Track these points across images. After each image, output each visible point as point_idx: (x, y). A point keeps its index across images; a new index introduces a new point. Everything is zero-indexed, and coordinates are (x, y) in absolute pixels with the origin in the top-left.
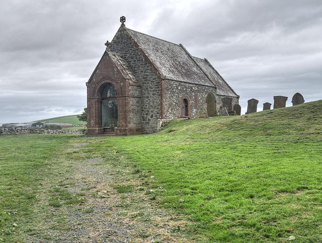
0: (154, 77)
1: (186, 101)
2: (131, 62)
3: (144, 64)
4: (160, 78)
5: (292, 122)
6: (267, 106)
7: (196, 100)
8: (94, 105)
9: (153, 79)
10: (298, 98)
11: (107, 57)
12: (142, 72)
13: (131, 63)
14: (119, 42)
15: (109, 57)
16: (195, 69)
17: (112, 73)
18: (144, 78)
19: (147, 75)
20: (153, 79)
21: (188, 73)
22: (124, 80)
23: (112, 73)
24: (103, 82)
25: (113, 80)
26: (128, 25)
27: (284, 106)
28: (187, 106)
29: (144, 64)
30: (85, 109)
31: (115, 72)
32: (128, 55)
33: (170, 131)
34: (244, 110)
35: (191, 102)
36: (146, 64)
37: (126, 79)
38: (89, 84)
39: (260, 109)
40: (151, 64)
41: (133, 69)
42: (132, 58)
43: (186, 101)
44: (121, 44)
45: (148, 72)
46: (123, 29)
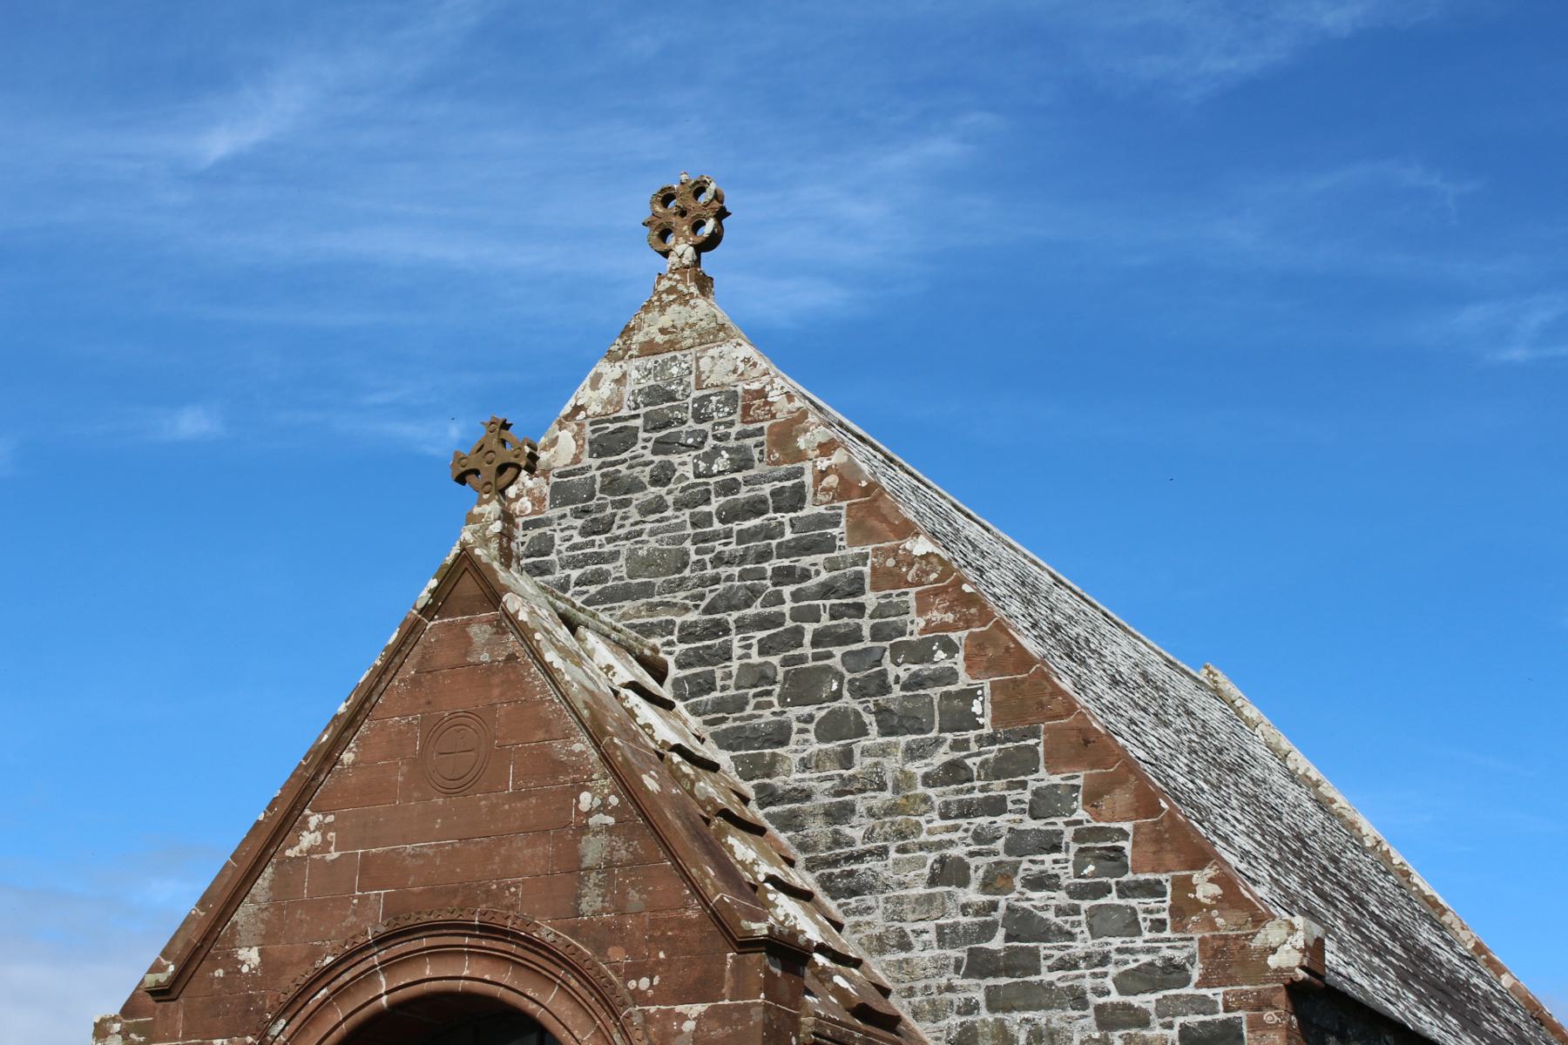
0: (1145, 948)
2: (780, 735)
3: (996, 770)
9: (1128, 983)
11: (480, 632)
12: (949, 872)
13: (790, 753)
14: (614, 485)
17: (534, 855)
18: (980, 965)
19: (1024, 925)
20: (1128, 983)
23: (534, 855)
24: (383, 992)
29: (996, 770)
31: (593, 850)
32: (744, 650)
36: (1013, 766)
41: (817, 829)
42: (803, 687)
44: (658, 506)
45: (1041, 882)
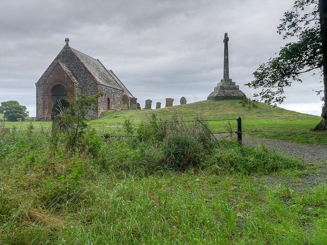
1: (109, 99)
4: (96, 83)
5: (194, 111)
6: (159, 105)
7: (114, 99)
8: (47, 100)
10: (183, 100)
15: (60, 66)
16: (110, 77)
19: (86, 81)
21: (108, 81)
22: (72, 83)
25: (63, 83)
26: (70, 45)
27: (172, 105)
28: (109, 103)
30: (231, 80)
33: (116, 117)
34: (143, 106)
35: (111, 100)
37: (74, 83)
38: (38, 85)
39: (154, 107)
40: (90, 73)
42: (75, 68)
43: (109, 99)
46: (67, 47)
